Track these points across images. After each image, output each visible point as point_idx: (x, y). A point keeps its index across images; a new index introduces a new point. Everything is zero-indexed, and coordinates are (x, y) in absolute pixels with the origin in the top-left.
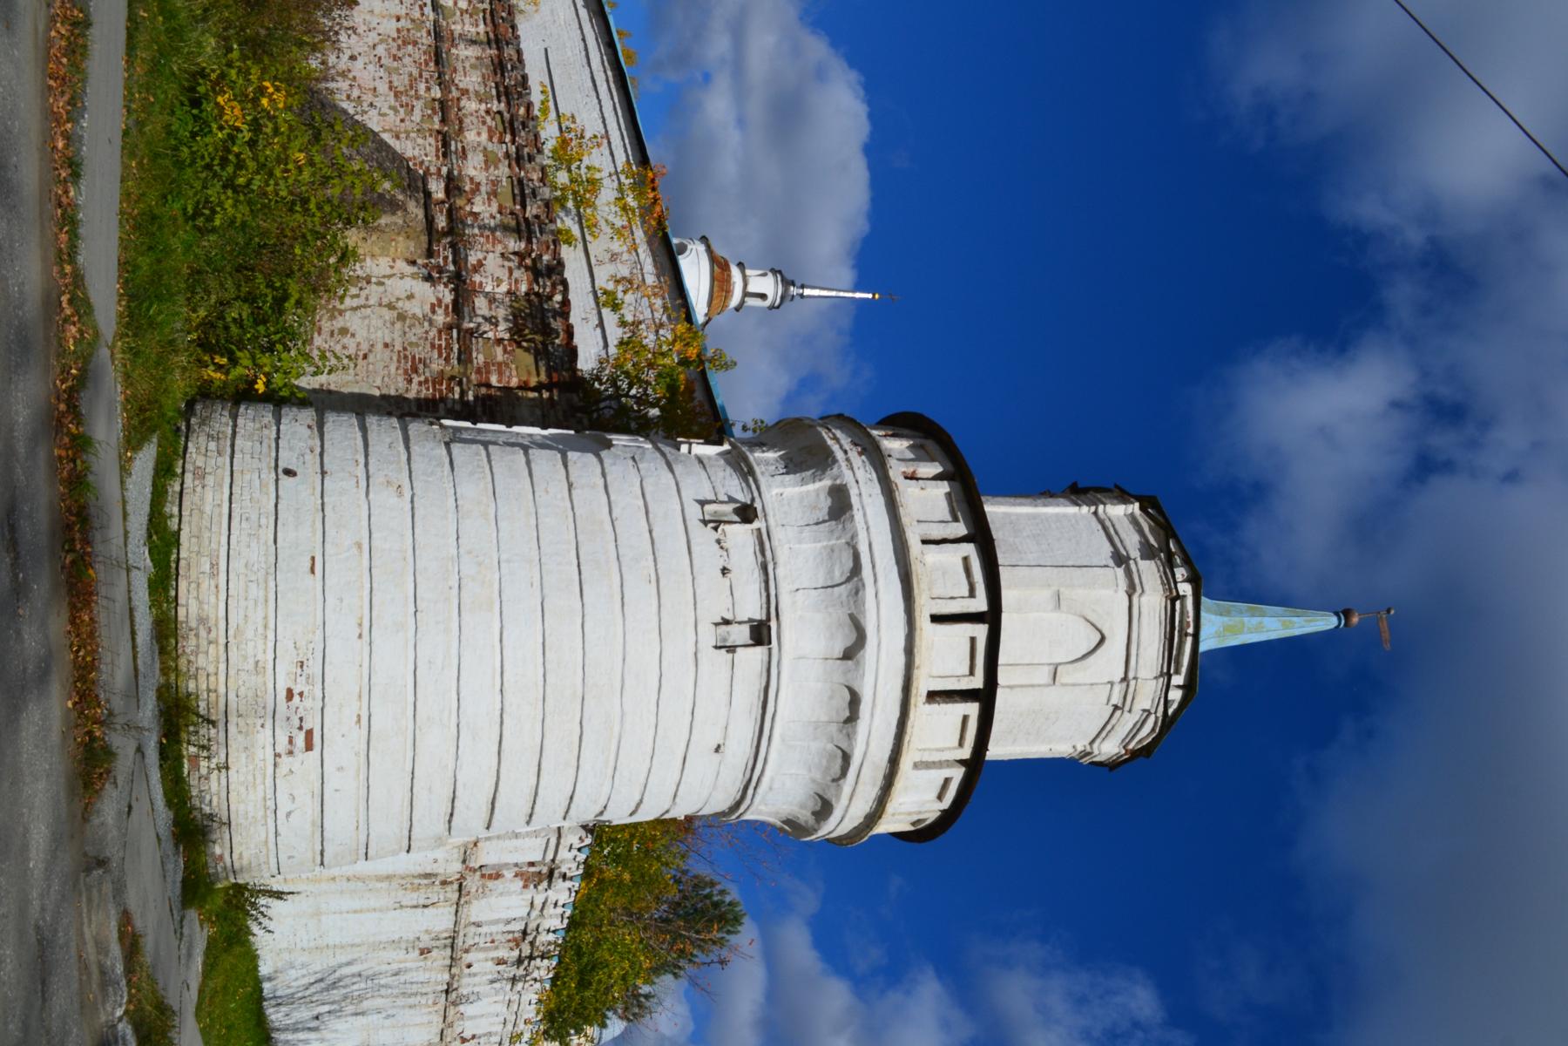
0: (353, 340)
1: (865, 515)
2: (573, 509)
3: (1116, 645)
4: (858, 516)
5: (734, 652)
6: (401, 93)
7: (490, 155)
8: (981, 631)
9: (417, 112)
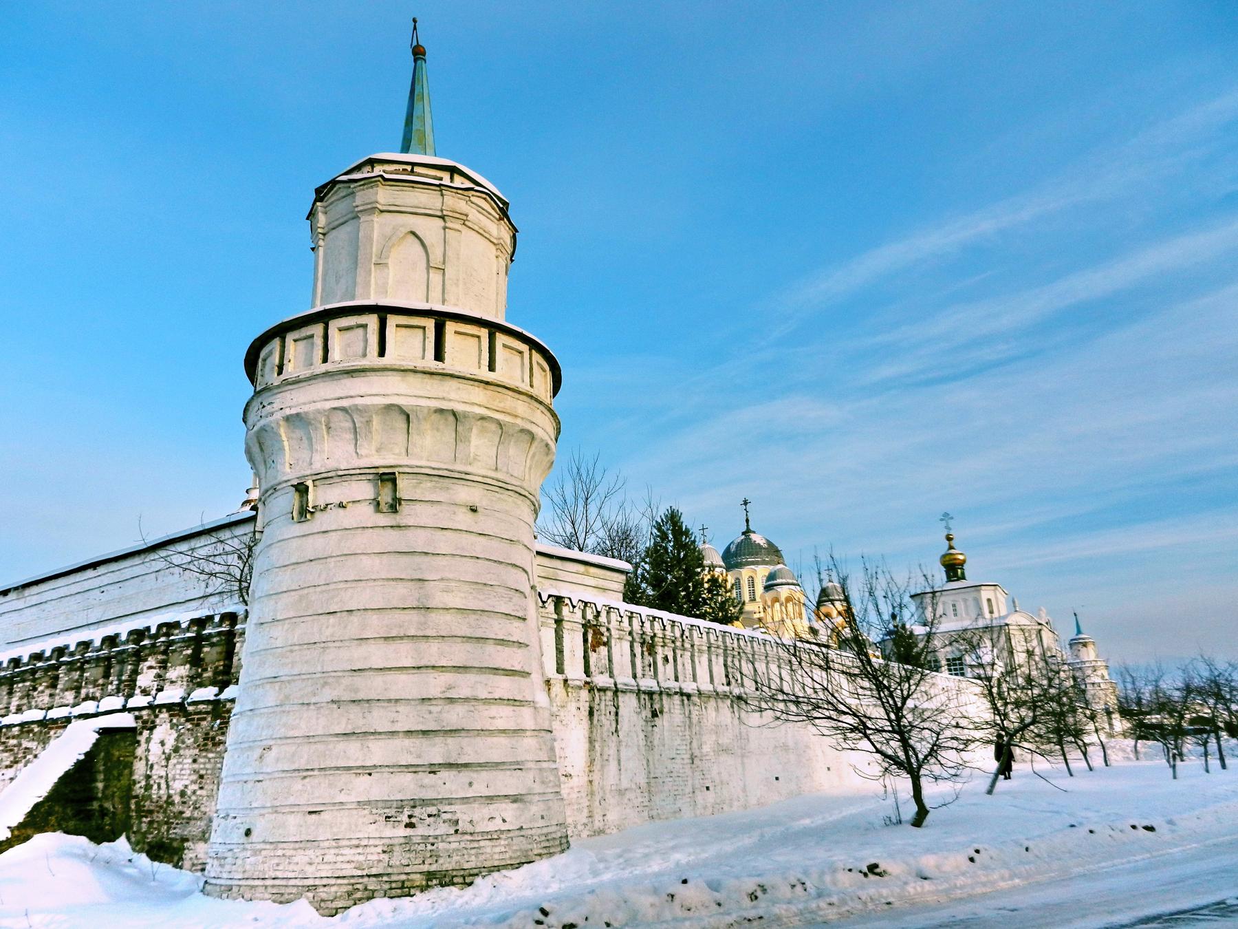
0: (189, 787)
1: (305, 404)
2: (290, 618)
3: (420, 224)
4: (305, 409)
5: (400, 500)
6: (15, 758)
7: (67, 686)
8: (392, 320)
9: (29, 745)
